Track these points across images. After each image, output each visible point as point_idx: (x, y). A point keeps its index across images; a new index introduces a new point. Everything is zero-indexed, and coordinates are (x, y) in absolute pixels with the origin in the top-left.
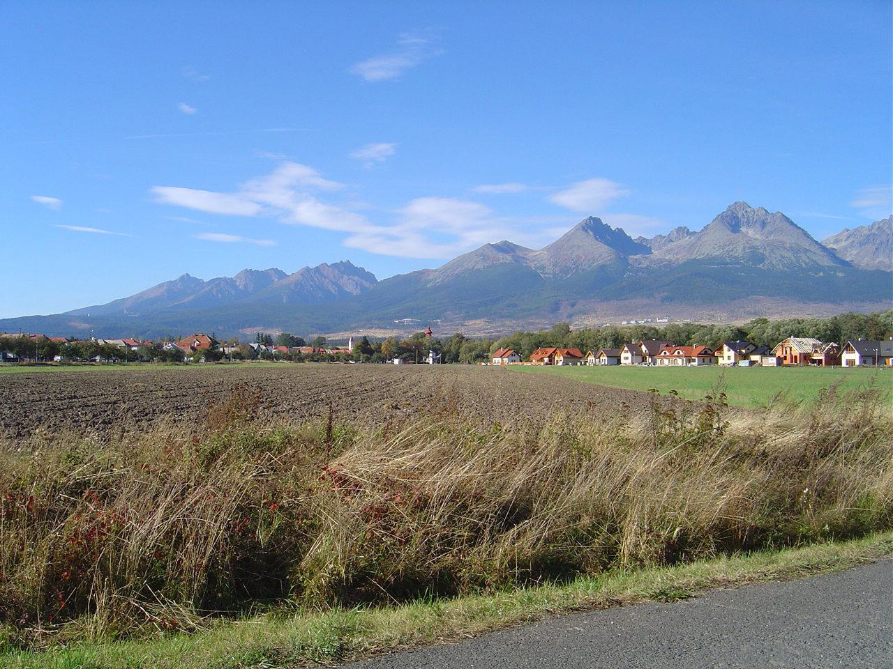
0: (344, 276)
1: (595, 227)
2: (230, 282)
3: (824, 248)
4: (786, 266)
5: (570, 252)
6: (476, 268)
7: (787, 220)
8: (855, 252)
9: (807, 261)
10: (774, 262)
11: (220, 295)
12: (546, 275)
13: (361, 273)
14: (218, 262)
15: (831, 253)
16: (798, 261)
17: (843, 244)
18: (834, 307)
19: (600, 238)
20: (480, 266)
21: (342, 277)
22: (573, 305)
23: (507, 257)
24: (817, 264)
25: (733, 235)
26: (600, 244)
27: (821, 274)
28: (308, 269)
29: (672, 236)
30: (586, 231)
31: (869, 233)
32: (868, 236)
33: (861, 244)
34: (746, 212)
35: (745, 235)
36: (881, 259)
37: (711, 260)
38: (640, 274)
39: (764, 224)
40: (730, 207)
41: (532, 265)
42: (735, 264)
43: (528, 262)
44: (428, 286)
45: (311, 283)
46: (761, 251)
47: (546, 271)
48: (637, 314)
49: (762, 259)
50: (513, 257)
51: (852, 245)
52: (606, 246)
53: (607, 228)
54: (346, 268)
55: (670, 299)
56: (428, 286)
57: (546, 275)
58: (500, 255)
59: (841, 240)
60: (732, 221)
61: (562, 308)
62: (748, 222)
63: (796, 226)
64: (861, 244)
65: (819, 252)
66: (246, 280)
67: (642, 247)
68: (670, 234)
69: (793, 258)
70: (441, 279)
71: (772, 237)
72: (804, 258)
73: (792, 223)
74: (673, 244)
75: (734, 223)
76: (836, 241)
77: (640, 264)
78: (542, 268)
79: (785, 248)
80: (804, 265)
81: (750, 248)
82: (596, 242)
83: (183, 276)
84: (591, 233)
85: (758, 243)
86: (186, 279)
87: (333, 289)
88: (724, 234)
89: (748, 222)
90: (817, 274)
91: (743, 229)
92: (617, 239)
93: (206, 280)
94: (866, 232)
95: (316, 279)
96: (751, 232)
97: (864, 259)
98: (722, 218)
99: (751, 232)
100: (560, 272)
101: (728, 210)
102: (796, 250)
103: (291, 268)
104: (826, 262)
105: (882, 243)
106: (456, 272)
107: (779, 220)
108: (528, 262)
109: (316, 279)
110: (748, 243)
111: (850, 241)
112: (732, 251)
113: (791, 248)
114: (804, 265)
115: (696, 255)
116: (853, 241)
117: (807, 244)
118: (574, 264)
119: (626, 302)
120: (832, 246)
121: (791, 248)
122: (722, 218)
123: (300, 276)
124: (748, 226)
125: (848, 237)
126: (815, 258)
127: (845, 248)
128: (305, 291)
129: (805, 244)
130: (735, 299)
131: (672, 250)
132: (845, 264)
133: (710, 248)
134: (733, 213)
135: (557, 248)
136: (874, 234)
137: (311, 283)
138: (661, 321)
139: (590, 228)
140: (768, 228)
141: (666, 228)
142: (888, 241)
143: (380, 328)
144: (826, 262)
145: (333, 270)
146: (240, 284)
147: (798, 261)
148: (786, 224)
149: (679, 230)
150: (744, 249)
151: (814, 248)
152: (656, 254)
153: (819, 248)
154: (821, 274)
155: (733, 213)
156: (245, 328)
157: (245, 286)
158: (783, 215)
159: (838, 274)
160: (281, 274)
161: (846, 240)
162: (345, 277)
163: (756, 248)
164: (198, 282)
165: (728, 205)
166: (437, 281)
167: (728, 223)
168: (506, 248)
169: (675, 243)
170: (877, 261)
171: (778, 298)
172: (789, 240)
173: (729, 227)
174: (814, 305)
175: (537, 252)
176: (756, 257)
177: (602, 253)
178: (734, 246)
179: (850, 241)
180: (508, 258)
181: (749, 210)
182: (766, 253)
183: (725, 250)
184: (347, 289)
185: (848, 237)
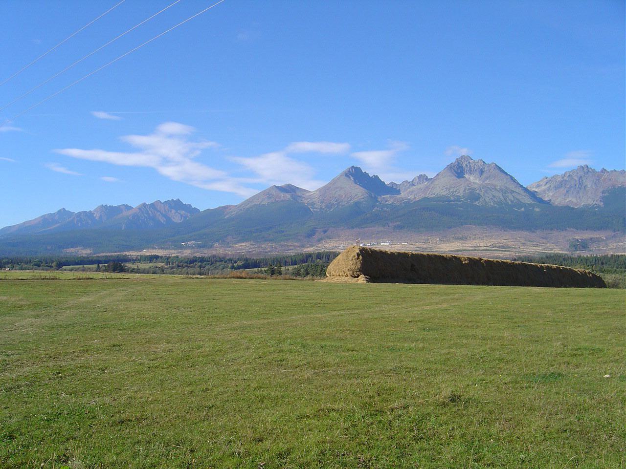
0: (172, 210)
1: (356, 174)
2: (89, 215)
3: (526, 190)
4: (496, 203)
5: (334, 192)
6: (263, 203)
7: (500, 169)
8: (552, 194)
9: (513, 199)
10: (487, 200)
11: (79, 224)
12: (315, 210)
13: (188, 208)
14: (84, 201)
15: (533, 195)
16: (505, 199)
17: (543, 188)
18: (528, 234)
19: (358, 182)
20: (265, 203)
21: (171, 211)
22: (325, 232)
23: (287, 195)
24: (520, 202)
25: (459, 180)
26: (357, 186)
27: (523, 209)
28: (144, 205)
29: (414, 181)
30: (348, 177)
31: (562, 180)
32: (562, 181)
33: (556, 188)
34: (469, 163)
35: (467, 180)
36: (570, 199)
37: (439, 199)
38: (385, 209)
39: (482, 172)
40: (457, 159)
41: (306, 202)
42: (457, 201)
43: (303, 199)
44: (225, 218)
45: (146, 215)
46: (478, 192)
47: (315, 206)
48: (372, 238)
49: (478, 197)
50: (292, 196)
51: (549, 189)
52: (362, 188)
53: (366, 175)
54: (177, 204)
55: (400, 227)
56: (225, 218)
57: (315, 210)
58: (282, 195)
59: (541, 185)
60: (458, 170)
61: (317, 234)
62: (470, 170)
63: (506, 173)
64: (556, 188)
65: (522, 192)
66: (100, 213)
67: (393, 189)
68: (413, 180)
69: (502, 198)
70: (235, 212)
71: (487, 181)
72: (510, 197)
73: (503, 171)
74: (414, 187)
75: (459, 171)
76: (538, 186)
77: (386, 201)
78: (313, 204)
79: (496, 190)
80: (510, 203)
81: (469, 189)
82: (355, 185)
83: (60, 210)
84: (352, 178)
85: (476, 186)
86: (63, 212)
87: (162, 220)
88: (450, 179)
89: (470, 170)
90: (519, 209)
91: (467, 176)
92: (372, 184)
93: (67, 210)
94: (560, 179)
95: (150, 212)
96: (472, 178)
97: (559, 199)
98: (450, 167)
99: (472, 178)
100: (326, 207)
101: (456, 162)
102: (504, 191)
103: (135, 204)
104: (527, 200)
105: (571, 187)
106: (247, 207)
107: (493, 169)
108: (303, 199)
109: (150, 212)
110: (468, 186)
111: (548, 185)
112: (456, 192)
113: (501, 189)
114: (510, 203)
115: (429, 195)
116: (550, 186)
117: (514, 187)
118: (336, 201)
119: (366, 229)
120: (534, 189)
121: (501, 189)
122: (451, 168)
123: (138, 210)
124: (470, 173)
125: (547, 183)
126: (518, 197)
127: (544, 191)
128: (140, 221)
129: (512, 187)
130: (451, 228)
131: (412, 192)
132: (541, 201)
133: (439, 190)
134: (459, 163)
135: (324, 190)
136: (566, 181)
137: (146, 215)
138: (384, 244)
139: (352, 175)
140: (484, 175)
141: (410, 177)
142: (575, 185)
143: (162, 248)
144: (527, 200)
145: (164, 205)
146: (97, 216)
147: (505, 199)
148: (498, 171)
149: (420, 177)
150: (465, 190)
151: (518, 190)
152: (403, 195)
153: (522, 190)
154: (523, 209)
155: (459, 163)
156: (69, 248)
157: (101, 217)
158: (496, 165)
159: (535, 209)
160: (128, 208)
161: (545, 185)
162: (174, 211)
163: (474, 189)
164: (70, 213)
165: (456, 158)
166: (232, 214)
167: (455, 171)
168: (289, 189)
169: (416, 187)
170: (567, 200)
171: (485, 227)
172: (499, 183)
173: (456, 175)
174: (512, 232)
175: (312, 192)
176: (474, 196)
177: (358, 192)
178: (458, 188)
179: (548, 185)
180: (288, 196)
181: (471, 161)
182: (482, 194)
183: (450, 191)
184: (173, 220)
185: (547, 183)
